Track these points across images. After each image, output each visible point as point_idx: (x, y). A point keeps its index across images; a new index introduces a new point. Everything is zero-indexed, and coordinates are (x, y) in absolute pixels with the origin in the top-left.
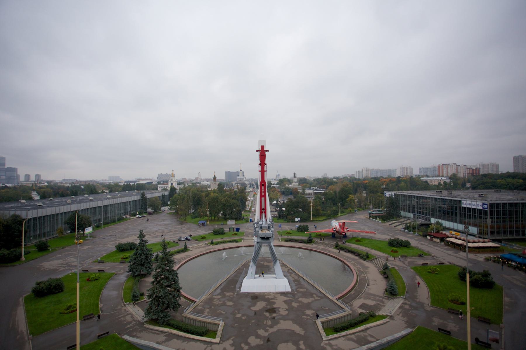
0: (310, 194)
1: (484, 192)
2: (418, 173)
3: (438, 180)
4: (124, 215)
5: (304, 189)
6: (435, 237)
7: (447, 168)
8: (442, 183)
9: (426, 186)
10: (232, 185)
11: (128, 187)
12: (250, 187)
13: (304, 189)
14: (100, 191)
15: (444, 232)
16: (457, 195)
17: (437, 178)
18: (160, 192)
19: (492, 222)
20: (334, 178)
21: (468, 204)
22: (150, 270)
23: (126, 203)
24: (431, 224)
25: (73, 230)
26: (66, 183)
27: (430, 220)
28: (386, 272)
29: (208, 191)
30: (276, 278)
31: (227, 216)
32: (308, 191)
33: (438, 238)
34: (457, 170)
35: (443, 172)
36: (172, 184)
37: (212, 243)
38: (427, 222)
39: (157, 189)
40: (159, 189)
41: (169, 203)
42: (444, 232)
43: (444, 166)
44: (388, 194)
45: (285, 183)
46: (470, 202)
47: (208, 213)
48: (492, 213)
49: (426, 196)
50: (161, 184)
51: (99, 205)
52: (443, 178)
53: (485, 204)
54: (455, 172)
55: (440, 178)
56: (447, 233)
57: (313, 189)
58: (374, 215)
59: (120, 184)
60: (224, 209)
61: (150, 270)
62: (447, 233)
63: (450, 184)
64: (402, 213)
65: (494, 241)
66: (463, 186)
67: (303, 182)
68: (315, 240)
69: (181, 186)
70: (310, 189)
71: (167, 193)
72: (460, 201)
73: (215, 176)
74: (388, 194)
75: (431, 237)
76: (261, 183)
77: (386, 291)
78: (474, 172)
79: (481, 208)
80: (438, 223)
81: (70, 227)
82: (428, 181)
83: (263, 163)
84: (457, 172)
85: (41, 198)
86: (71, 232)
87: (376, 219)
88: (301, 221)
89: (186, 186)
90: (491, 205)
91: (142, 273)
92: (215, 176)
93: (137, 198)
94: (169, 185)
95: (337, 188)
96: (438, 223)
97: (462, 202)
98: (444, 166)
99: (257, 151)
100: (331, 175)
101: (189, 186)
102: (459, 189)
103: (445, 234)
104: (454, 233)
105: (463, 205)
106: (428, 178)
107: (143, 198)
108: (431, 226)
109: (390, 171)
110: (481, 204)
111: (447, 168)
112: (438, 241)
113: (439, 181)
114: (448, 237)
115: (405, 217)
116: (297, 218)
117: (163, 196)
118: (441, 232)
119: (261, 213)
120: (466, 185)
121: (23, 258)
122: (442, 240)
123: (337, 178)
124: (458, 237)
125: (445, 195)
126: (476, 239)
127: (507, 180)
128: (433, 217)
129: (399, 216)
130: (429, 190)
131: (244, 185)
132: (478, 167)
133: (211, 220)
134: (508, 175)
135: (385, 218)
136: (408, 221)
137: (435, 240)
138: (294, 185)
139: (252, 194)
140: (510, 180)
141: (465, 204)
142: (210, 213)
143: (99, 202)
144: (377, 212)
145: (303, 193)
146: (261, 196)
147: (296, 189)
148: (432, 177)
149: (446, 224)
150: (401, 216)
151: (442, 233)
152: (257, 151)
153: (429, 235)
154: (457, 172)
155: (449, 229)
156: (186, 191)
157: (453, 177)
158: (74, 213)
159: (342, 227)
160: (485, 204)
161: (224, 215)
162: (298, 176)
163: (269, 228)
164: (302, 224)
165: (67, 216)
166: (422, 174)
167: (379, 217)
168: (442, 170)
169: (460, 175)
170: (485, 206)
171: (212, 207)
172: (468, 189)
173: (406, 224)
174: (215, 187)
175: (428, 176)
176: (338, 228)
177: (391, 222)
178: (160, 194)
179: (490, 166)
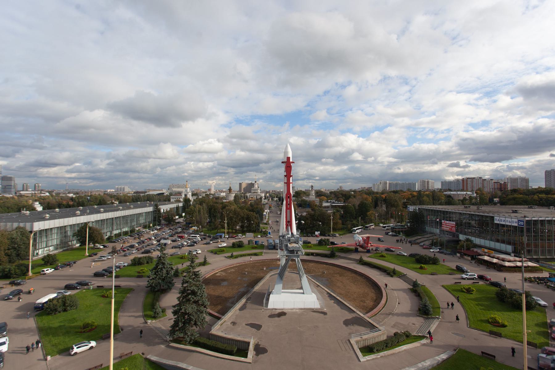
0: (328, 207)
1: (515, 207)
2: (440, 187)
3: (463, 194)
4: (137, 227)
5: (321, 202)
6: (465, 255)
7: (472, 183)
8: (467, 197)
9: (450, 200)
10: (247, 197)
11: (138, 199)
12: (265, 199)
13: (321, 202)
14: (108, 202)
15: (475, 250)
16: (486, 210)
17: (462, 193)
18: (172, 203)
19: (528, 240)
20: (351, 191)
21: (501, 220)
22: (170, 285)
23: (140, 214)
24: (460, 240)
25: (83, 243)
26: (69, 193)
27: (458, 237)
28: (416, 290)
29: (222, 203)
30: (303, 293)
31: (245, 229)
32: (325, 204)
33: (469, 255)
34: (483, 184)
35: (467, 186)
36: (186, 195)
37: (232, 257)
38: (455, 239)
39: (169, 200)
40: (172, 200)
41: (184, 214)
42: (475, 250)
43: (469, 180)
44: (411, 208)
45: (301, 195)
46: (504, 219)
47: (226, 225)
48: (528, 230)
49: (504, 223)
50: (174, 195)
51: (110, 217)
52: (469, 193)
53: (521, 221)
54: (480, 186)
55: (465, 193)
56: (479, 251)
57: (330, 202)
58: (397, 230)
59: (129, 195)
60: (242, 222)
61: (170, 285)
62: (479, 251)
63: (476, 198)
64: (428, 229)
65: (531, 260)
66: (491, 202)
67: (319, 194)
68: (337, 254)
69: (195, 197)
70: (327, 202)
71: (181, 205)
72: (493, 217)
73: (230, 188)
74: (411, 208)
75: (461, 255)
76: (287, 195)
77: (419, 310)
78: (503, 186)
79: (516, 225)
80: (468, 240)
81: (79, 240)
82: (452, 196)
83: (288, 175)
84: (483, 186)
85: (43, 209)
86: (80, 246)
87: (399, 234)
88: (321, 234)
89: (200, 197)
90: (528, 222)
91: (162, 288)
92: (230, 188)
93: (150, 209)
94: (183, 196)
95: (356, 202)
96: (468, 240)
97: (495, 218)
98: (469, 180)
99: (282, 162)
100: (348, 186)
101: (203, 197)
102: (486, 204)
103: (477, 252)
104: (486, 250)
105: (496, 222)
106: (452, 193)
107: (157, 211)
108: (461, 243)
109: (409, 184)
110: (516, 220)
111: (472, 183)
112: (469, 258)
113: (464, 196)
114: (480, 255)
115: (431, 233)
116: (317, 231)
117: (177, 208)
118: (472, 249)
119: (287, 225)
120: (493, 201)
121: (30, 273)
122: (473, 258)
123: (354, 191)
124: (492, 255)
125: (473, 210)
126: (512, 258)
127: (540, 195)
128: (461, 233)
129: (424, 232)
130: (453, 205)
131: (259, 197)
132: (506, 181)
133: (228, 233)
134: (539, 191)
135: (409, 233)
136: (435, 237)
137: (466, 257)
138: (312, 197)
139: (267, 206)
140: (543, 196)
141: (499, 220)
142: (228, 226)
143: (110, 213)
144: (400, 227)
145: (321, 206)
146: (287, 209)
147: (314, 201)
148: (455, 191)
149: (477, 241)
150: (426, 232)
151: (473, 251)
152: (282, 162)
153: (459, 253)
154: (483, 186)
155: (480, 247)
156: (201, 202)
157: (479, 192)
158: (86, 224)
159: (366, 242)
160: (521, 221)
161: (242, 227)
162: (315, 188)
163: (296, 242)
164: (323, 238)
165: (77, 228)
166: (444, 188)
167: (402, 231)
168: (467, 184)
169: (486, 190)
170: (521, 223)
171: (230, 219)
172: (495, 204)
173: (433, 240)
174: (232, 197)
175: (451, 190)
176: (362, 242)
177: (416, 238)
178: (174, 206)
179: (519, 181)
